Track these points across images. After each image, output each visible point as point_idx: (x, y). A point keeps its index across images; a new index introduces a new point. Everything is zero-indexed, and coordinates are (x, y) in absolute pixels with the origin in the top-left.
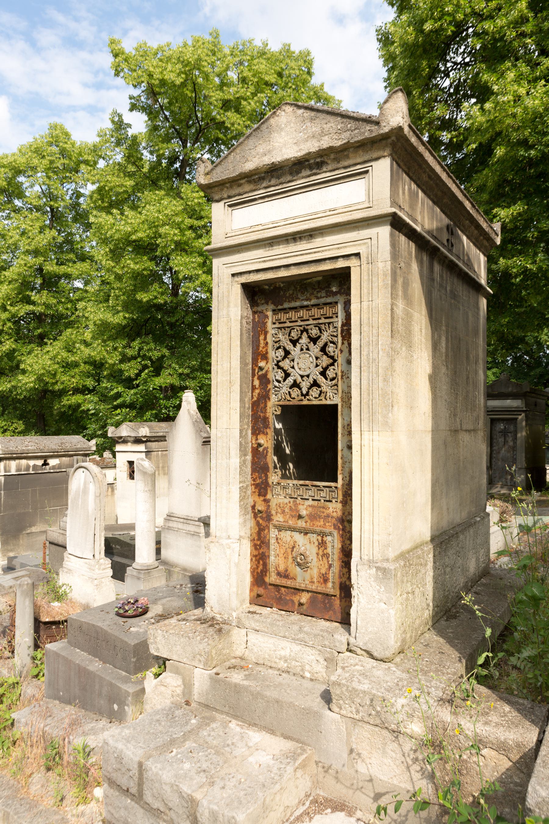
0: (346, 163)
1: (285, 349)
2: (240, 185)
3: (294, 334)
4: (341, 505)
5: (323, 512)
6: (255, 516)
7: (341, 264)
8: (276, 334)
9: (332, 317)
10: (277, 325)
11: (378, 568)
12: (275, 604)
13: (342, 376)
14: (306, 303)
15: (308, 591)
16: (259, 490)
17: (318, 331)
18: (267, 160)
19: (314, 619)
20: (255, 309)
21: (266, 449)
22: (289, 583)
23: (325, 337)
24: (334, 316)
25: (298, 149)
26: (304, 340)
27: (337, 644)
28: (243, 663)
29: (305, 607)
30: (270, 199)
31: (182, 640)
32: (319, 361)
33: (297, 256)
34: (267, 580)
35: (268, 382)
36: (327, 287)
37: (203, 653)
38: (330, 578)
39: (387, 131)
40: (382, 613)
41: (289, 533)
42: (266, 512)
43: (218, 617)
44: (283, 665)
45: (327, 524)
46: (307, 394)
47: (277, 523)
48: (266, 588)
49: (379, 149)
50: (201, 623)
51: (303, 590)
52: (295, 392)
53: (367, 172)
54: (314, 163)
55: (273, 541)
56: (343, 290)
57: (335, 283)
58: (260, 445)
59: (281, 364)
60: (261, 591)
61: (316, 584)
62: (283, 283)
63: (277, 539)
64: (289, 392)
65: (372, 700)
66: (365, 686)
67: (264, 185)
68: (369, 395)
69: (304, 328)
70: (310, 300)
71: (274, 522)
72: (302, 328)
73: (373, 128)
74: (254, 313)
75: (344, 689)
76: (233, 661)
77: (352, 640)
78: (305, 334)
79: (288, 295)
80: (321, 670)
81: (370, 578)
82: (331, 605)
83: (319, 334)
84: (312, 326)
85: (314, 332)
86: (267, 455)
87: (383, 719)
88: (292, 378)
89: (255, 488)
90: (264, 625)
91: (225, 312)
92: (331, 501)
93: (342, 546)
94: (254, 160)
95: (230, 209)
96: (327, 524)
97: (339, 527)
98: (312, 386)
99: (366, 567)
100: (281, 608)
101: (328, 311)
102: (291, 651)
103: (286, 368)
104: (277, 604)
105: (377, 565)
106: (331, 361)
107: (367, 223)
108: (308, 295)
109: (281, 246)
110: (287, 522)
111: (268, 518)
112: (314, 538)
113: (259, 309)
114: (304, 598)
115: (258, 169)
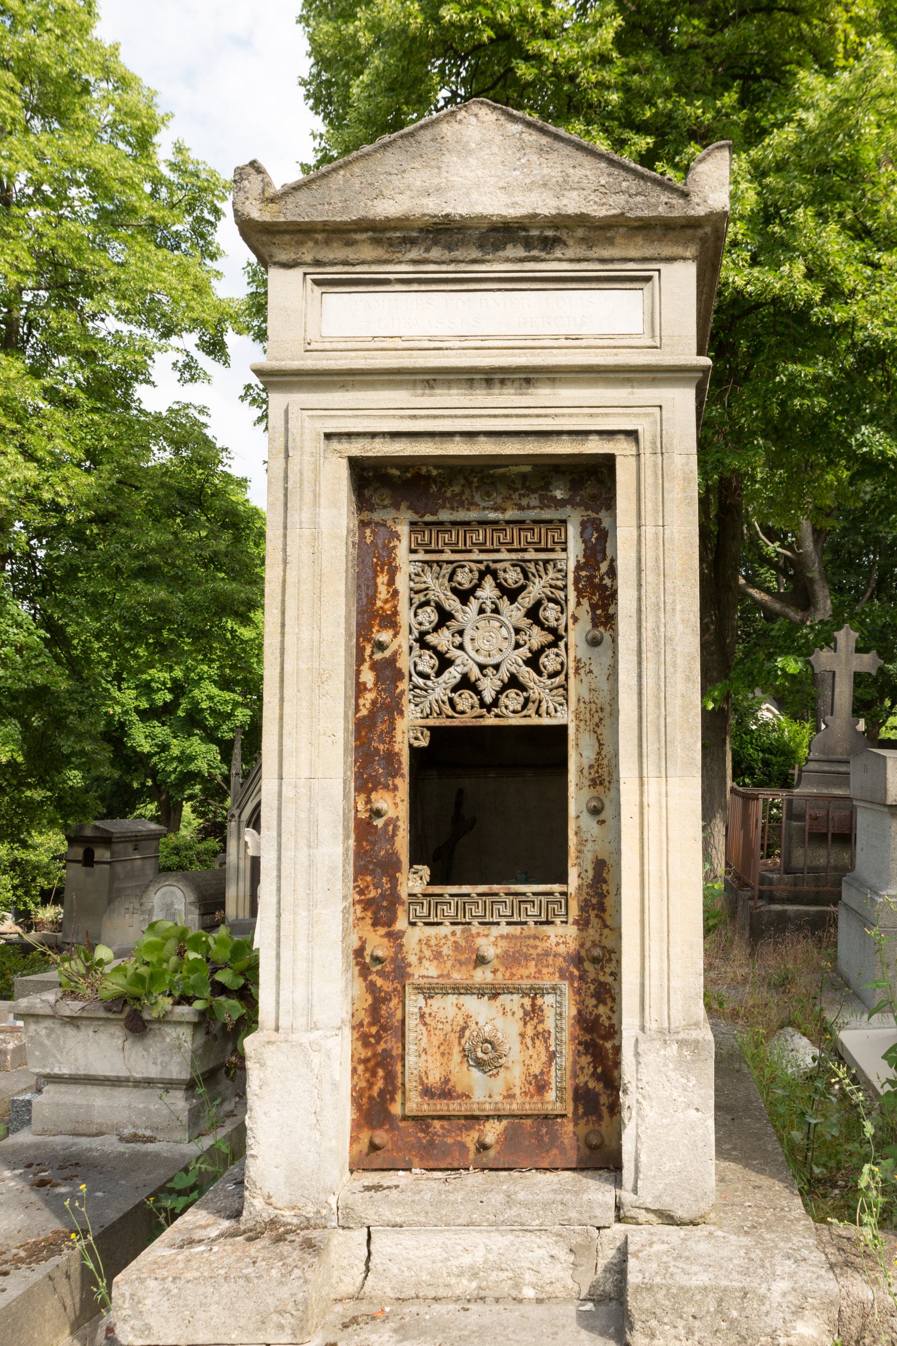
0: (606, 253)
1: (439, 608)
2: (350, 243)
3: (464, 579)
4: (576, 927)
5: (536, 947)
6: (364, 971)
7: (594, 447)
8: (417, 575)
9: (552, 550)
10: (421, 556)
11: (682, 1043)
12: (416, 1161)
13: (577, 669)
14: (492, 516)
15: (499, 1117)
16: (375, 913)
17: (521, 576)
18: (431, 205)
19: (515, 1174)
20: (366, 516)
21: (393, 822)
22: (454, 1107)
23: (536, 590)
24: (558, 548)
25: (509, 201)
26: (488, 591)
27: (598, 1212)
28: (364, 1308)
29: (492, 1153)
30: (423, 288)
31: (225, 1288)
32: (522, 638)
33: (495, 416)
34: (396, 1109)
35: (399, 675)
36: (542, 488)
37: (290, 1307)
38: (553, 1081)
39: (702, 214)
40: (692, 1129)
41: (452, 999)
42: (394, 960)
43: (288, 1216)
44: (467, 1286)
45: (545, 971)
46: (495, 703)
47: (422, 981)
48: (392, 1128)
49: (676, 242)
50: (250, 1239)
51: (488, 1117)
52: (466, 700)
53: (648, 279)
54: (539, 238)
55: (412, 1022)
56: (578, 499)
57: (590, 480)
58: (378, 813)
59: (429, 638)
60: (381, 1137)
61: (519, 1099)
62: (436, 467)
63: (422, 1016)
64: (451, 700)
65: (720, 1301)
66: (702, 1278)
67: (414, 254)
68: (659, 708)
69: (488, 567)
70: (504, 510)
71: (416, 980)
72: (482, 567)
73: (674, 201)
74: (363, 524)
75: (660, 1295)
76: (339, 1308)
77: (627, 1196)
78: (489, 579)
79: (449, 494)
80: (562, 1274)
81: (665, 1065)
82: (554, 1137)
83: (522, 581)
84: (507, 565)
85: (512, 577)
86: (394, 834)
87: (744, 1333)
88: (459, 669)
89: (365, 909)
90: (418, 1208)
91: (306, 516)
92: (552, 923)
93: (579, 1012)
94: (399, 198)
95: (318, 290)
96: (545, 971)
97: (571, 973)
98: (505, 688)
99: (658, 1044)
100: (432, 1165)
101: (548, 537)
102: (489, 1251)
103: (442, 648)
104: (422, 1158)
105: (681, 1036)
106: (551, 638)
107: (652, 375)
108: (499, 500)
109: (454, 391)
110: (448, 976)
111: (399, 970)
112: (513, 1002)
113: (377, 516)
114: (492, 1132)
115: (407, 219)
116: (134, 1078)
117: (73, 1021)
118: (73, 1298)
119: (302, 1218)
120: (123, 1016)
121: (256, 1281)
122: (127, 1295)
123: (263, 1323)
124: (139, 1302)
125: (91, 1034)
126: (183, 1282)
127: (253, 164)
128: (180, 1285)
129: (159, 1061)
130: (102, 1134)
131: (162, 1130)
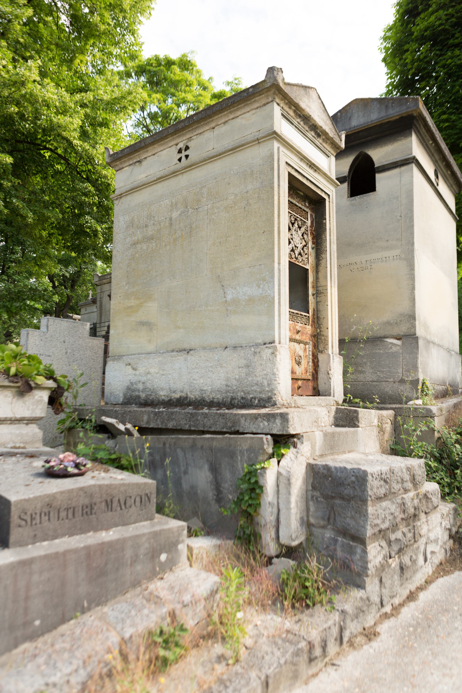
109: (155, 146)
127: (281, 69)
129: (30, 408)
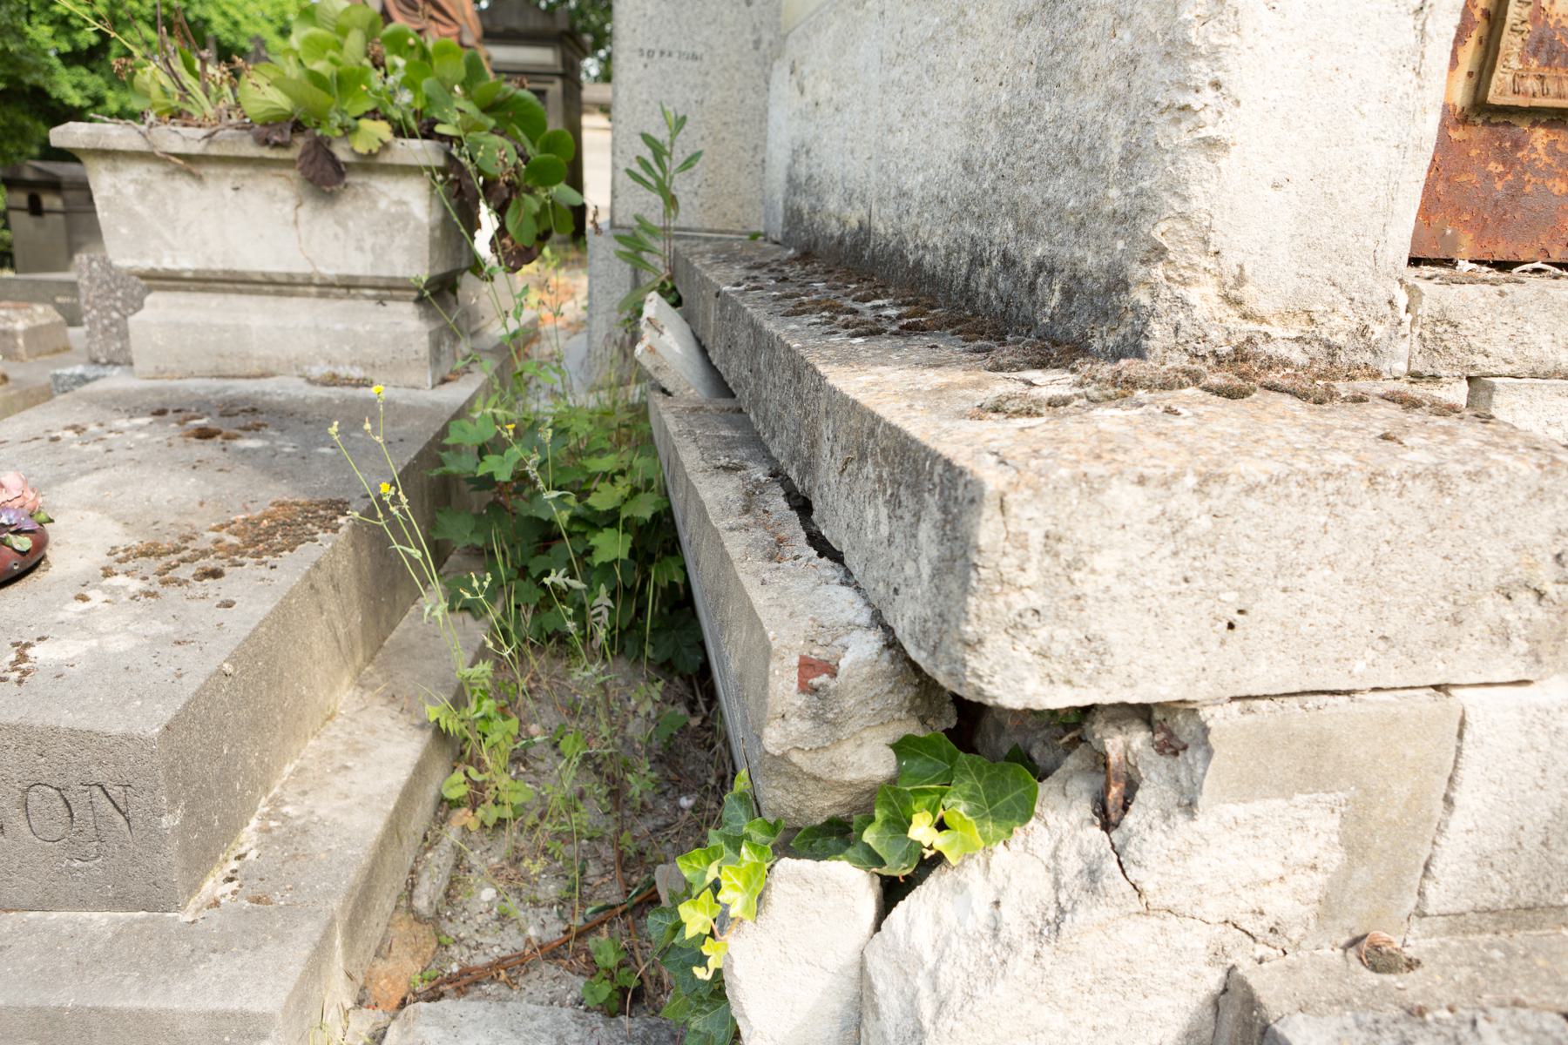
116: (322, 277)
117: (190, 164)
118: (347, 623)
119: (1316, 350)
120: (293, 154)
121: (1465, 487)
122: (1036, 537)
123: (1457, 622)
124: (1075, 564)
125: (229, 193)
126: (1230, 490)
128: (1219, 505)
129: (367, 245)
130: (272, 375)
131: (383, 367)
